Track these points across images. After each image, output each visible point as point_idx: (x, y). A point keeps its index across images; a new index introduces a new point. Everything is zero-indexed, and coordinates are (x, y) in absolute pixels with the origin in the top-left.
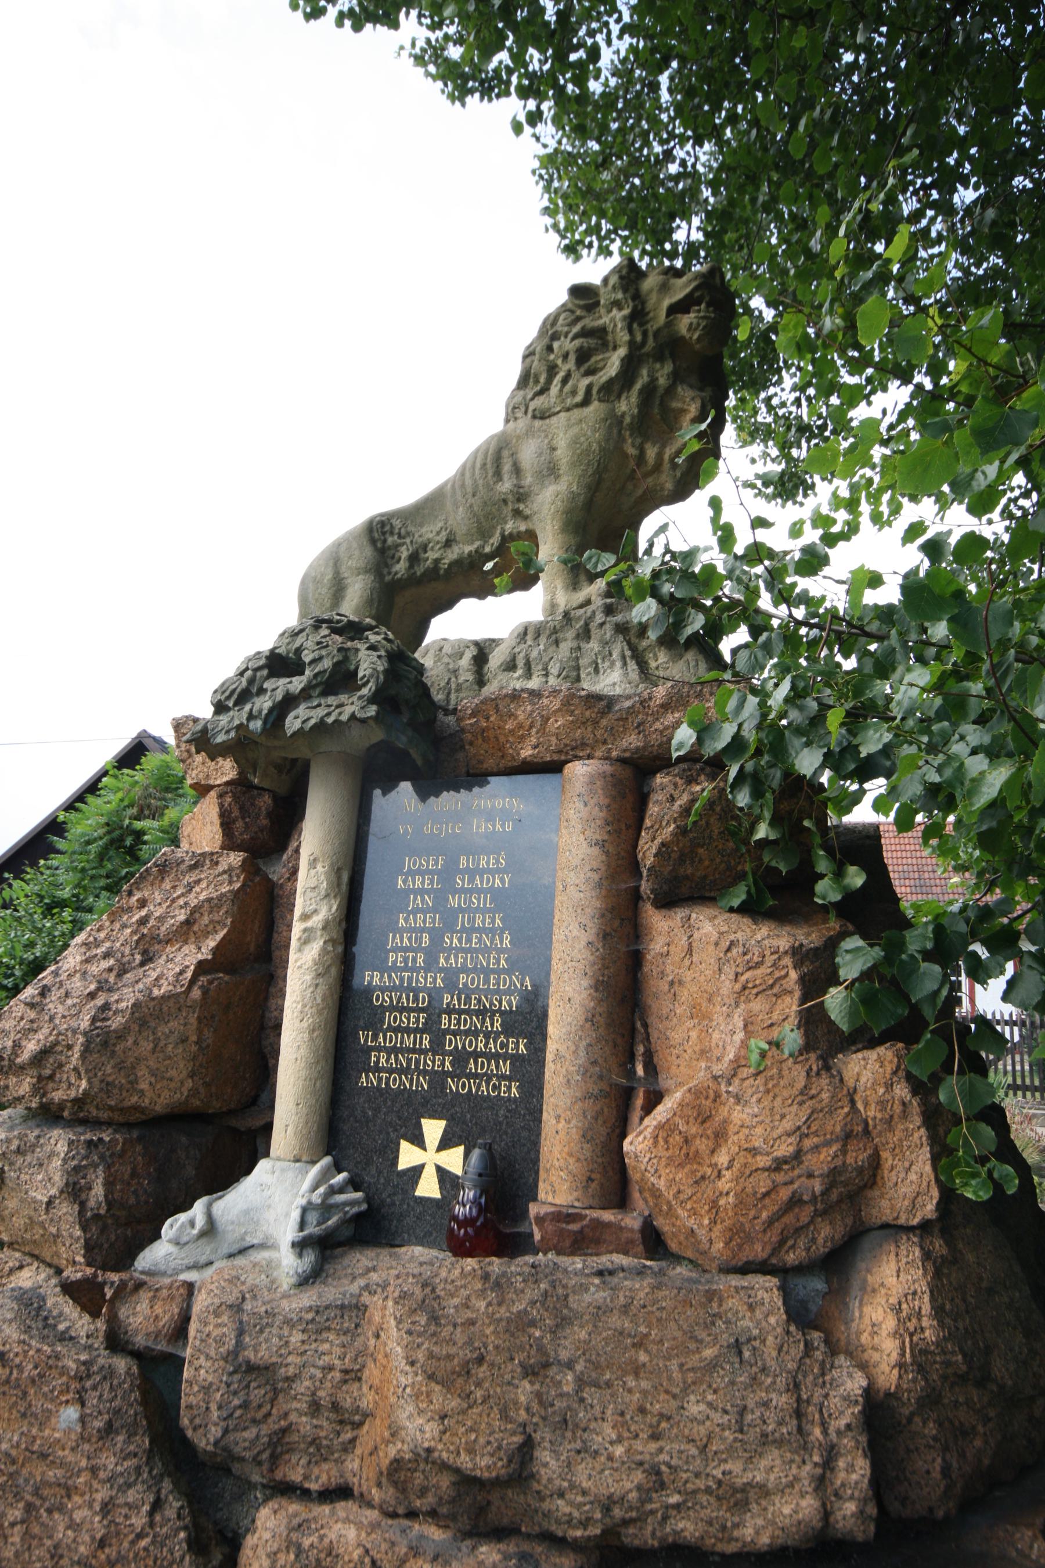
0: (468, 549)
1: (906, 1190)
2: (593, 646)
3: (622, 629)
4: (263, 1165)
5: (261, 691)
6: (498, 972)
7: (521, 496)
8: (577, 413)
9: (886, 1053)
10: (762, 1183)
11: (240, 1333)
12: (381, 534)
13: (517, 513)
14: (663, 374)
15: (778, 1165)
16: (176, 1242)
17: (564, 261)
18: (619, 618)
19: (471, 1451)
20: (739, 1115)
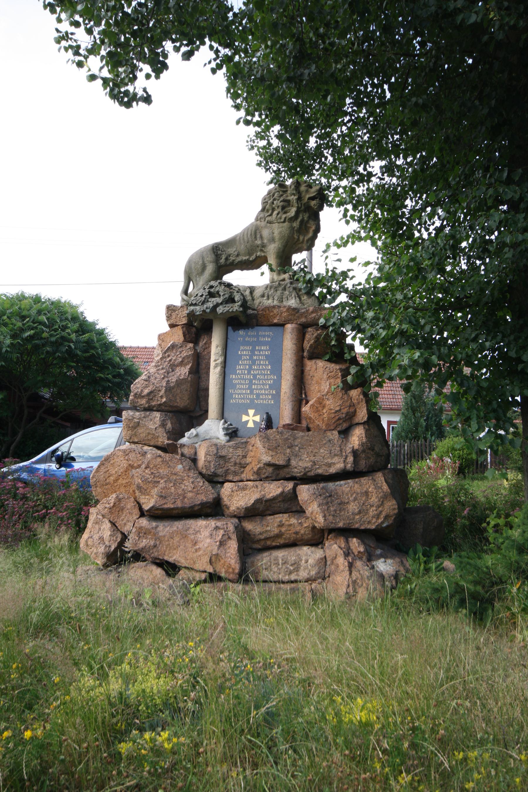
0: (244, 258)
1: (361, 416)
2: (287, 292)
3: (295, 289)
5: (208, 301)
6: (268, 375)
7: (264, 246)
8: (281, 225)
9: (359, 390)
10: (333, 415)
11: (217, 450)
12: (217, 250)
13: (262, 250)
16: (189, 438)
17: (234, 110)
18: (294, 286)
19: (278, 461)
20: (328, 403)
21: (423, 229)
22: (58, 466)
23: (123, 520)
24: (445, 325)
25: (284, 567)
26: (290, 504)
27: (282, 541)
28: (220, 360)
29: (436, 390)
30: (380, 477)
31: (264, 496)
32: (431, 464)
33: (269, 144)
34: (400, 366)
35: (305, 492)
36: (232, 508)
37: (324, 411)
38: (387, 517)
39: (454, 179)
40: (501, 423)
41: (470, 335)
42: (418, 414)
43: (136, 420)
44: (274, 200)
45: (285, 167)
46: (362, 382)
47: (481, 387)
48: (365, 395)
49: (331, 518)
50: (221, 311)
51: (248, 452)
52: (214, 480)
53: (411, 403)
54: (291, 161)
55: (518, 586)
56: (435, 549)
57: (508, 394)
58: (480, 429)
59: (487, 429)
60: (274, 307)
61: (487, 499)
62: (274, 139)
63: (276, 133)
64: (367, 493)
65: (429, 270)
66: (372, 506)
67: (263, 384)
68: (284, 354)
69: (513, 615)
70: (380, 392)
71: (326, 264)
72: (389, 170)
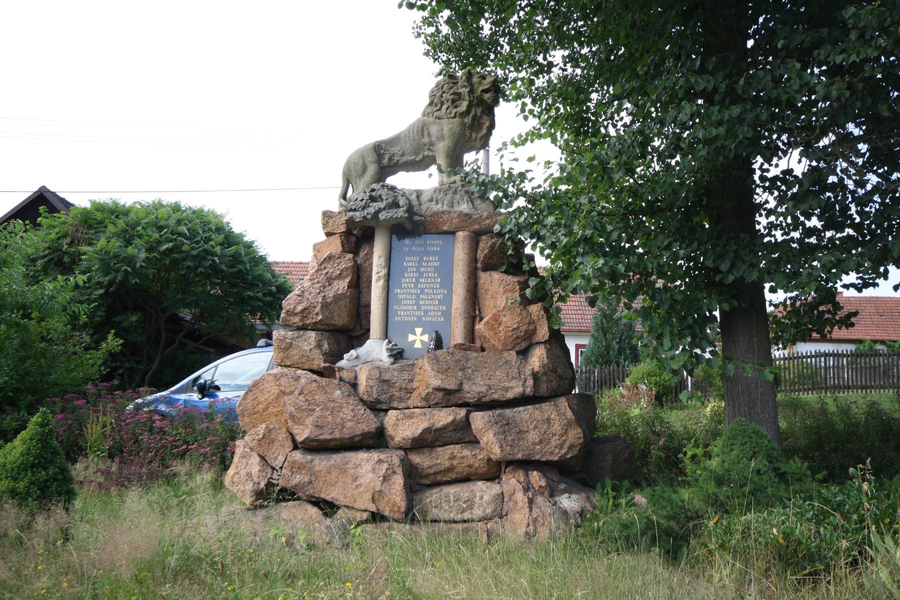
0: (410, 158)
1: (542, 334)
2: (458, 196)
3: (467, 192)
4: (368, 342)
6: (437, 289)
7: (432, 144)
9: (539, 304)
10: (510, 334)
11: (380, 373)
12: (379, 149)
13: (429, 149)
14: (479, 111)
15: (514, 329)
16: (348, 360)
20: (504, 319)
21: (610, 126)
22: (200, 396)
23: (273, 453)
24: (636, 232)
25: (456, 505)
26: (462, 433)
27: (453, 476)
28: (384, 272)
29: (625, 304)
30: (563, 402)
31: (433, 424)
32: (624, 392)
33: (438, 31)
34: (583, 277)
35: (479, 419)
36: (398, 439)
37: (501, 329)
38: (571, 447)
39: (641, 69)
40: (697, 340)
41: (663, 242)
42: (609, 336)
43: (288, 341)
44: (444, 92)
45: (456, 57)
46: (542, 296)
47: (675, 301)
48: (546, 310)
49: (508, 448)
50: (384, 217)
51: (414, 375)
52: (377, 407)
53: (602, 323)
54: (463, 50)
55: (715, 520)
56: (626, 483)
57: (705, 308)
58: (673, 347)
59: (681, 347)
60: (443, 212)
61: (685, 428)
62: (444, 25)
63: (445, 18)
64: (548, 421)
65: (616, 170)
66: (554, 435)
67: (432, 300)
68: (455, 265)
69: (710, 552)
70: (563, 308)
71: (502, 164)
72: (573, 59)
